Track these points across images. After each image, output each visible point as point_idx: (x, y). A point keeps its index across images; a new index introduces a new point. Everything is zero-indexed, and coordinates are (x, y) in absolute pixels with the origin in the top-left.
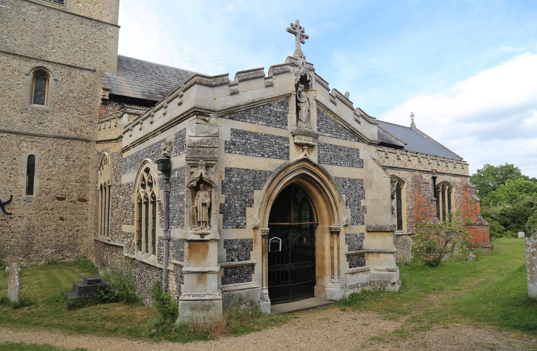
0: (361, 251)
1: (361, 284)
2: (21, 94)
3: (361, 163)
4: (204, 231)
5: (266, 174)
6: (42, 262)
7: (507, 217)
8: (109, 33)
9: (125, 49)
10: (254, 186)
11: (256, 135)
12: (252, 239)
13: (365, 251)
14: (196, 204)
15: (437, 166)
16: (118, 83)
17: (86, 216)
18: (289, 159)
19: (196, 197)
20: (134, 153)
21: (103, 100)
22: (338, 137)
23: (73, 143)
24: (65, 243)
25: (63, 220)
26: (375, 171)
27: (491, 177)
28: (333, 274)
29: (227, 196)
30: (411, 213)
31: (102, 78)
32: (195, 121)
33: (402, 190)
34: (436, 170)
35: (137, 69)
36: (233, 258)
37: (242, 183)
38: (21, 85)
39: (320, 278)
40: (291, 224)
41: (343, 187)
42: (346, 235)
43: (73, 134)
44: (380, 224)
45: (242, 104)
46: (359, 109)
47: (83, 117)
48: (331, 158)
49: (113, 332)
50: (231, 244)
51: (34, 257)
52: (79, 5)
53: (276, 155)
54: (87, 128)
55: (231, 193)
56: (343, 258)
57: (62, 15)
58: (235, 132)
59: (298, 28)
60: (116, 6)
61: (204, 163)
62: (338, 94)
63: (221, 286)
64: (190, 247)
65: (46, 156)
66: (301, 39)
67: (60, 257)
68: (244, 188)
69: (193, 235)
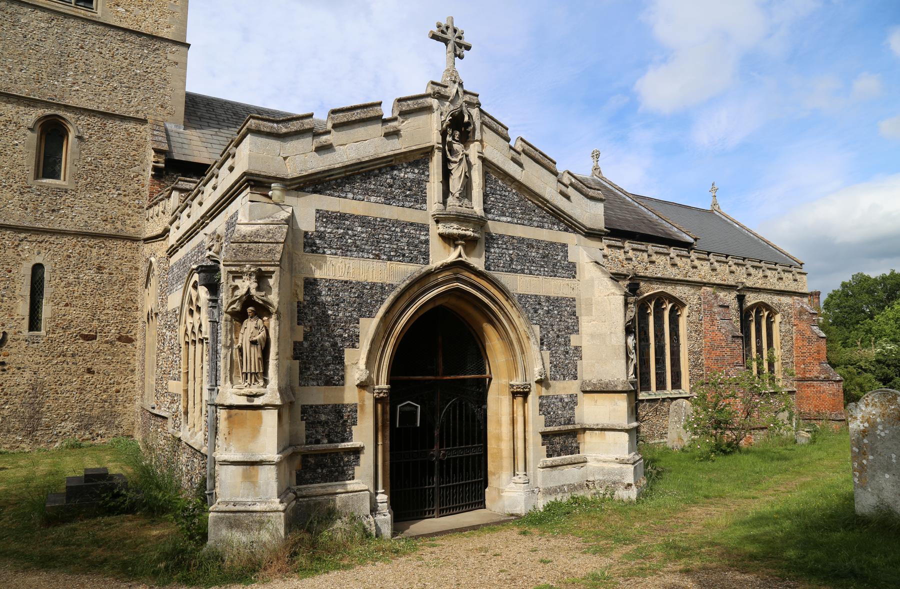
0: (570, 427)
1: (568, 485)
2: (20, 162)
3: (571, 270)
4: (254, 389)
5: (384, 289)
6: (57, 445)
7: (888, 366)
8: (170, 56)
9: (198, 83)
10: (359, 310)
11: (364, 221)
12: (356, 405)
13: (578, 427)
14: (240, 342)
15: (745, 276)
16: (185, 141)
17: (131, 367)
18: (428, 263)
19: (242, 331)
20: (181, 257)
21: (155, 169)
22: (526, 222)
23: (110, 243)
24: (96, 412)
25: (93, 373)
26: (596, 282)
27: (866, 297)
28: (467, 470)
29: (308, 329)
30: (698, 359)
31: (155, 133)
32: (248, 198)
33: (681, 319)
34: (743, 283)
35: (224, 117)
36: (319, 437)
37: (337, 305)
38: (20, 147)
39: (494, 474)
40: (438, 378)
41: (536, 312)
42: (540, 397)
43: (108, 229)
44: (606, 378)
45: (337, 166)
46: (569, 173)
47: (126, 199)
48: (512, 260)
49: (93, 567)
50: (315, 412)
51: (42, 436)
52: (120, 9)
53: (404, 255)
54: (134, 218)
55: (315, 323)
56: (535, 439)
57: (90, 28)
58: (323, 216)
59: (450, 31)
60: (182, 10)
61: (252, 270)
62: (527, 147)
63: (295, 488)
64: (229, 417)
65: (63, 265)
66: (455, 50)
67: (87, 436)
68: (341, 315)
69: (234, 396)
